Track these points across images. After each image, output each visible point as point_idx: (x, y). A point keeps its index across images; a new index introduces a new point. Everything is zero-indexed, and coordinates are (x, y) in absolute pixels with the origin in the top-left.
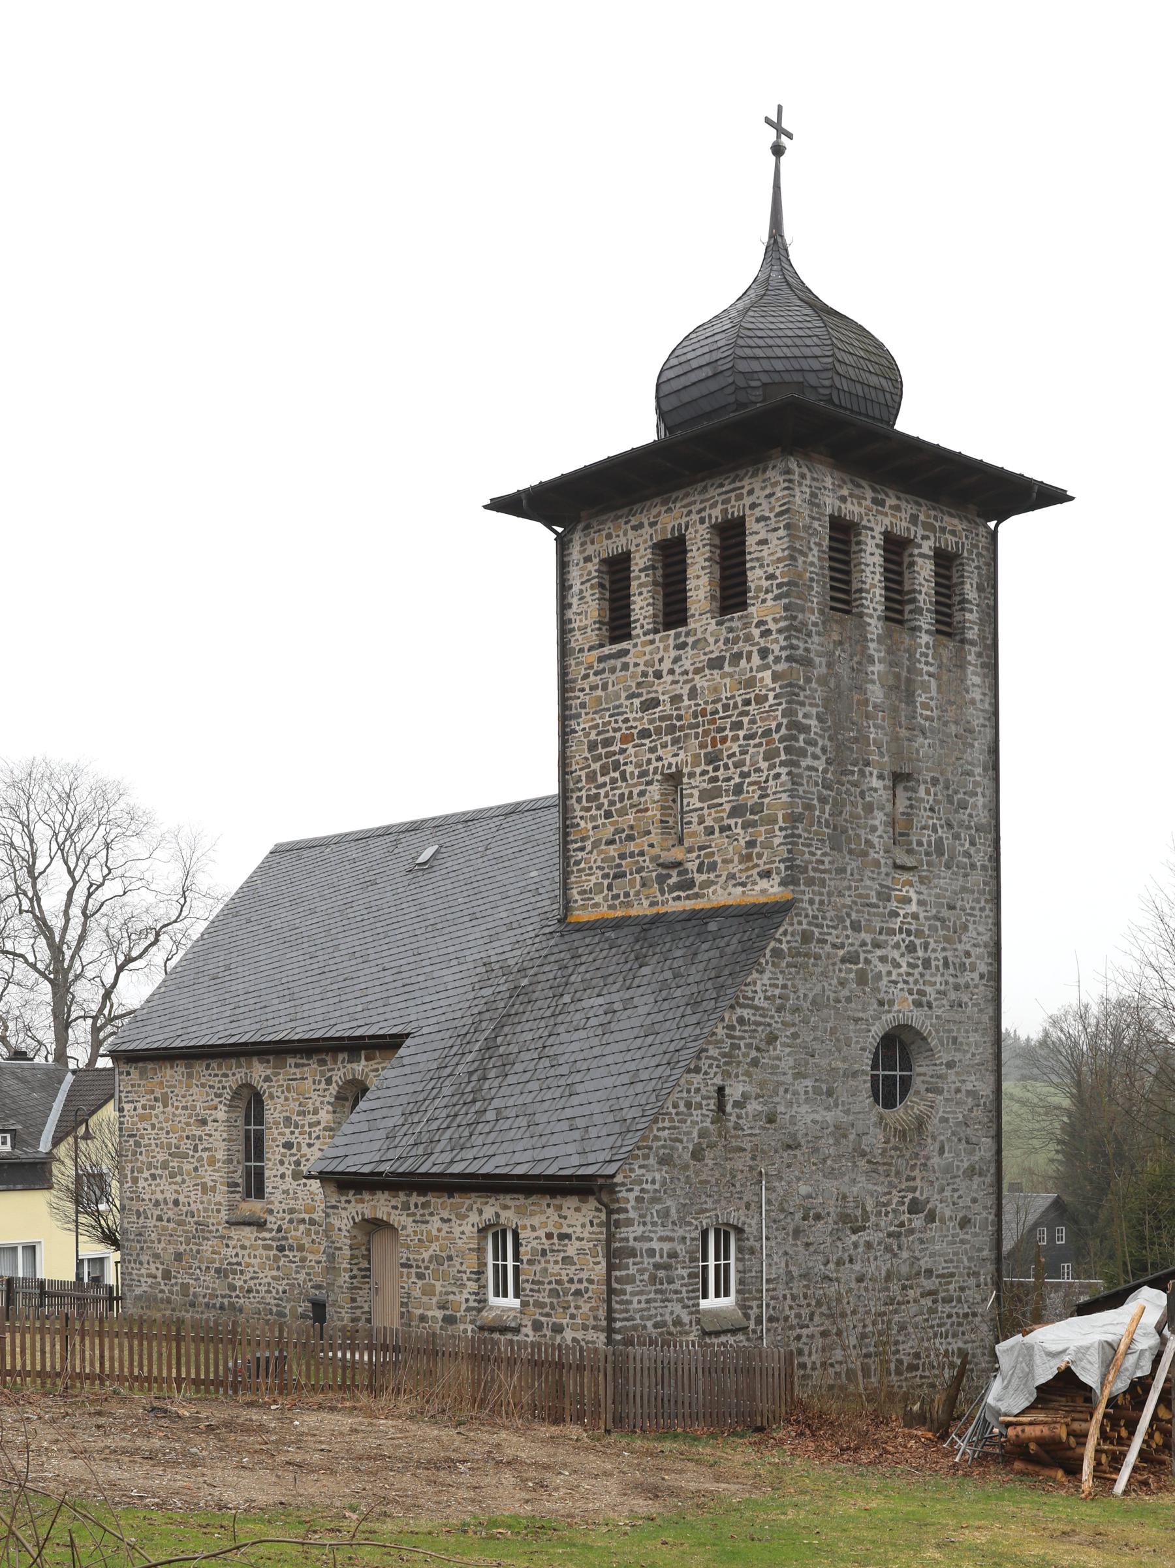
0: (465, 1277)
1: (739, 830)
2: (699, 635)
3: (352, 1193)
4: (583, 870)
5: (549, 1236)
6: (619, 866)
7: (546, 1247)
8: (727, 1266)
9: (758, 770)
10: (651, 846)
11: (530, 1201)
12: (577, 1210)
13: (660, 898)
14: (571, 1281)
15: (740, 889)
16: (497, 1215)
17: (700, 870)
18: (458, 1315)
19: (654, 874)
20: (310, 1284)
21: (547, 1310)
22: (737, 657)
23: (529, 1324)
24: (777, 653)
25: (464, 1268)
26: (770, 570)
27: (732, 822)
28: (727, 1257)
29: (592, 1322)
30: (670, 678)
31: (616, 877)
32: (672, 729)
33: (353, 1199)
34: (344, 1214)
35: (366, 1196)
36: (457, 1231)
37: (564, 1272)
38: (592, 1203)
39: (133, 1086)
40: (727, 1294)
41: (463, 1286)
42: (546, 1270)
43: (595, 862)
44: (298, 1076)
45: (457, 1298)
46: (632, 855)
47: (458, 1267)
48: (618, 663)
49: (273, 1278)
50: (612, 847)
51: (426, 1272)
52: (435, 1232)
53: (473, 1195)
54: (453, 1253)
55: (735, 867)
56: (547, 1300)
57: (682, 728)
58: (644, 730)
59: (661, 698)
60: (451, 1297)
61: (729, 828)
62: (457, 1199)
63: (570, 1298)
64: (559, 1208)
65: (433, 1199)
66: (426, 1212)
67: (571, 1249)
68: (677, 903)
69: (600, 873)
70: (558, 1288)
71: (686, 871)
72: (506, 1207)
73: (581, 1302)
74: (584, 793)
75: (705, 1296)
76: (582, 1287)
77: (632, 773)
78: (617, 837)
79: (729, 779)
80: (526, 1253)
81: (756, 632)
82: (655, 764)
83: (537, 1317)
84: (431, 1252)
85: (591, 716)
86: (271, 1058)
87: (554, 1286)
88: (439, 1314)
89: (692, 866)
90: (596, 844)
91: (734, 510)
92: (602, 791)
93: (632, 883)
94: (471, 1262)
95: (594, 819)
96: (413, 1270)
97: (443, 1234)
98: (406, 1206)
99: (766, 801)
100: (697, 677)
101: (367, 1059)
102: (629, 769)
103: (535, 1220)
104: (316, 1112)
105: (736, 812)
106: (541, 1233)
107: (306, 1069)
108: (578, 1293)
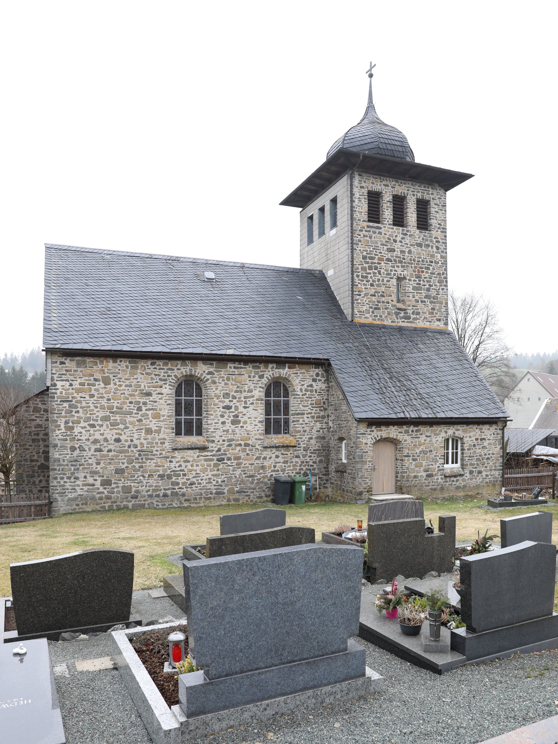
0: (438, 458)
1: (428, 303)
2: (412, 233)
3: (374, 427)
4: (360, 303)
5: (477, 439)
6: (377, 305)
7: (476, 443)
8: (457, 453)
9: (436, 285)
10: (392, 301)
11: (469, 427)
12: (489, 429)
13: (396, 320)
14: (485, 455)
15: (429, 323)
16: (454, 433)
17: (413, 314)
18: (434, 473)
19: (393, 311)
20: (244, 476)
21: (475, 466)
22: (428, 246)
23: (468, 472)
24: (442, 249)
25: (438, 454)
26: (439, 222)
27: (426, 300)
28: (457, 449)
29: (494, 468)
30: (400, 244)
31: (375, 309)
32: (401, 262)
33: (375, 430)
34: (369, 437)
35: (383, 428)
36: (434, 440)
37: (483, 452)
38: (494, 426)
39: (67, 371)
40: (456, 463)
41: (437, 461)
42: (475, 452)
43: (366, 301)
44: (237, 373)
45: (434, 466)
46: (383, 302)
47: (435, 454)
48: (377, 231)
49: (213, 475)
50: (374, 297)
51: (418, 458)
52: (423, 441)
53: (442, 426)
54: (432, 449)
55: (427, 315)
56: (475, 463)
57: (405, 263)
58: (388, 258)
59: (396, 250)
60: (431, 466)
61: (425, 302)
62: (435, 428)
63: (485, 461)
64: (482, 429)
65: (422, 428)
66: (418, 433)
67: (486, 443)
68: (403, 323)
69: (368, 306)
70: (480, 458)
71: (407, 313)
72: (458, 430)
73: (489, 462)
74: (360, 274)
75: (447, 463)
76: (489, 456)
77: (383, 273)
78: (376, 294)
79: (425, 285)
80: (467, 446)
81: (434, 240)
82: (394, 272)
83: (471, 469)
84: (420, 449)
85: (363, 246)
86: (214, 363)
87: (478, 457)
88: (424, 474)
89: (410, 312)
90: (366, 295)
91: (426, 197)
92: (369, 276)
93: (384, 313)
94: (442, 451)
95: (365, 285)
96: (411, 458)
97: (427, 442)
98: (407, 432)
99: (439, 296)
100: (412, 247)
101: (289, 368)
102: (382, 271)
103: (471, 434)
104: (250, 391)
105: (426, 297)
106: (474, 439)
107: (243, 370)
108: (488, 458)
